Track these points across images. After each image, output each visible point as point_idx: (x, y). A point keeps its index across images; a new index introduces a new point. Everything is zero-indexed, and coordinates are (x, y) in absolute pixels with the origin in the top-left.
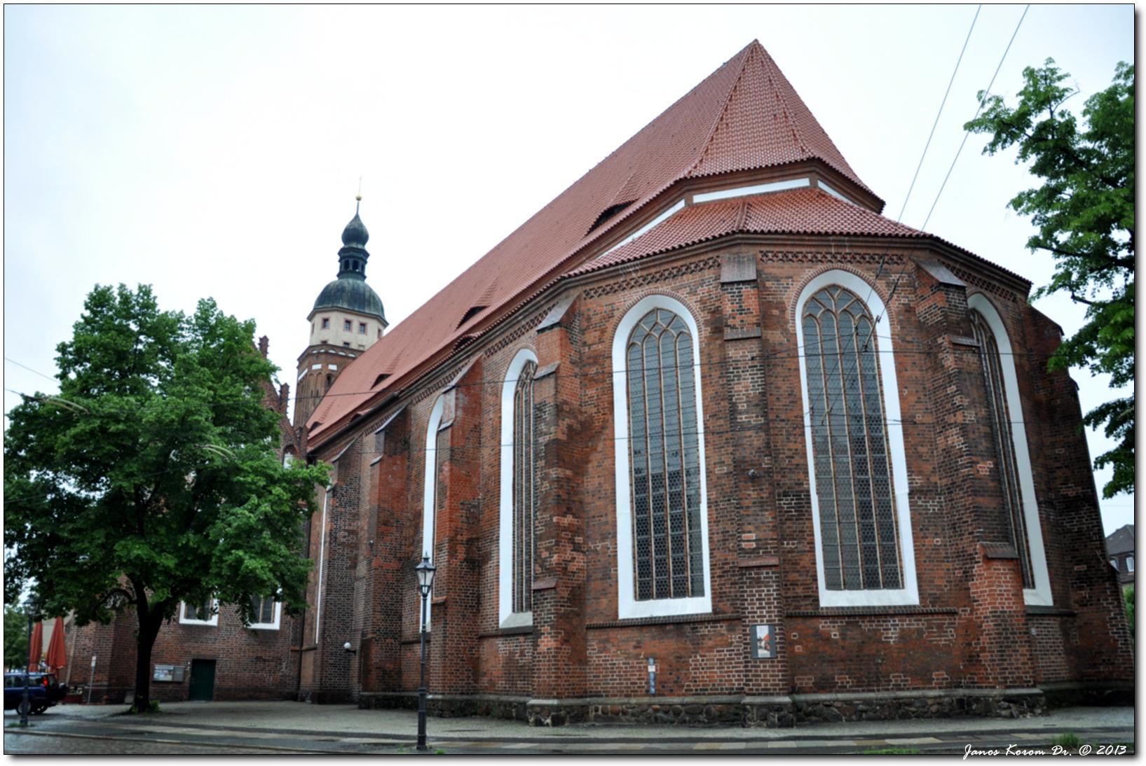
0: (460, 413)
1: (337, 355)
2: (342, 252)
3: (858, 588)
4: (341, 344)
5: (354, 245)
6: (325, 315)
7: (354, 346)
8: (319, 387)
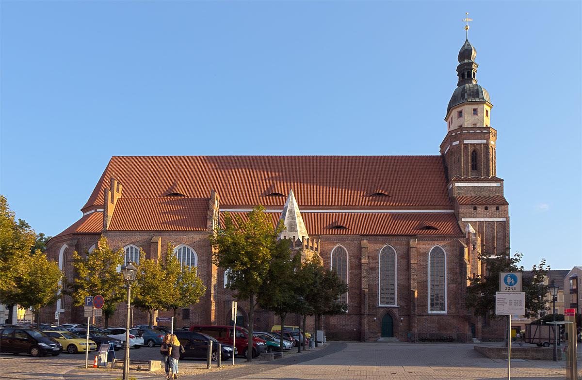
3: (504, 226)
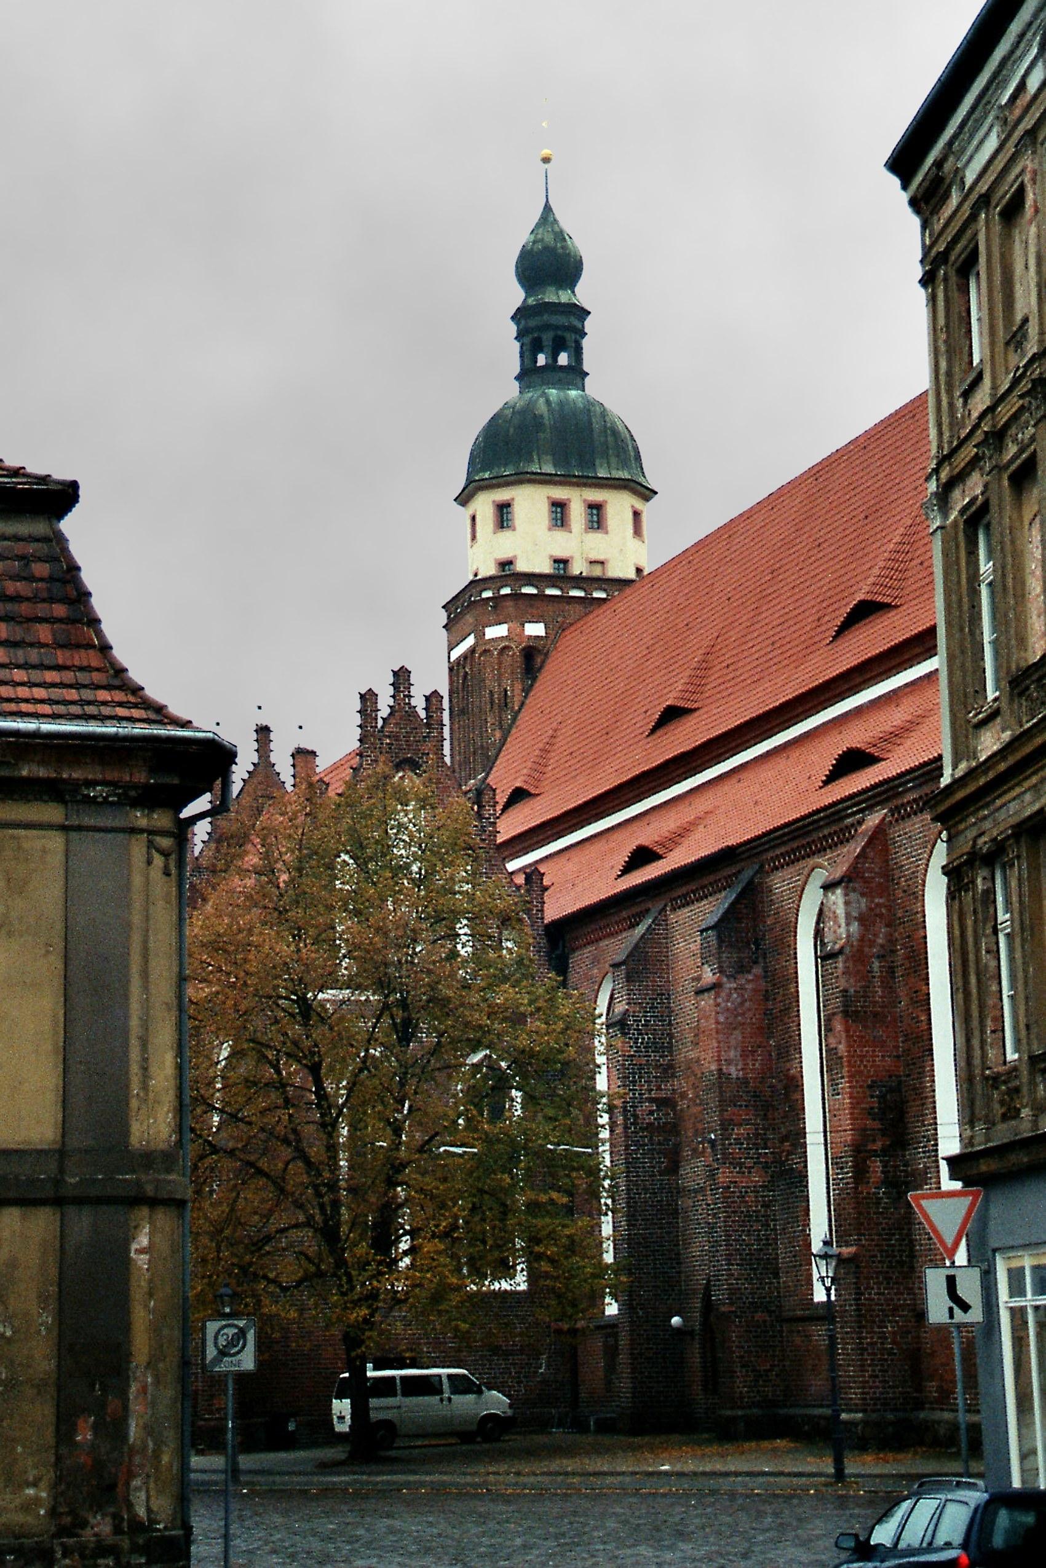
0: (855, 927)
1: (541, 597)
2: (520, 315)
4: (546, 568)
5: (551, 296)
6: (502, 495)
7: (578, 568)
8: (507, 684)
